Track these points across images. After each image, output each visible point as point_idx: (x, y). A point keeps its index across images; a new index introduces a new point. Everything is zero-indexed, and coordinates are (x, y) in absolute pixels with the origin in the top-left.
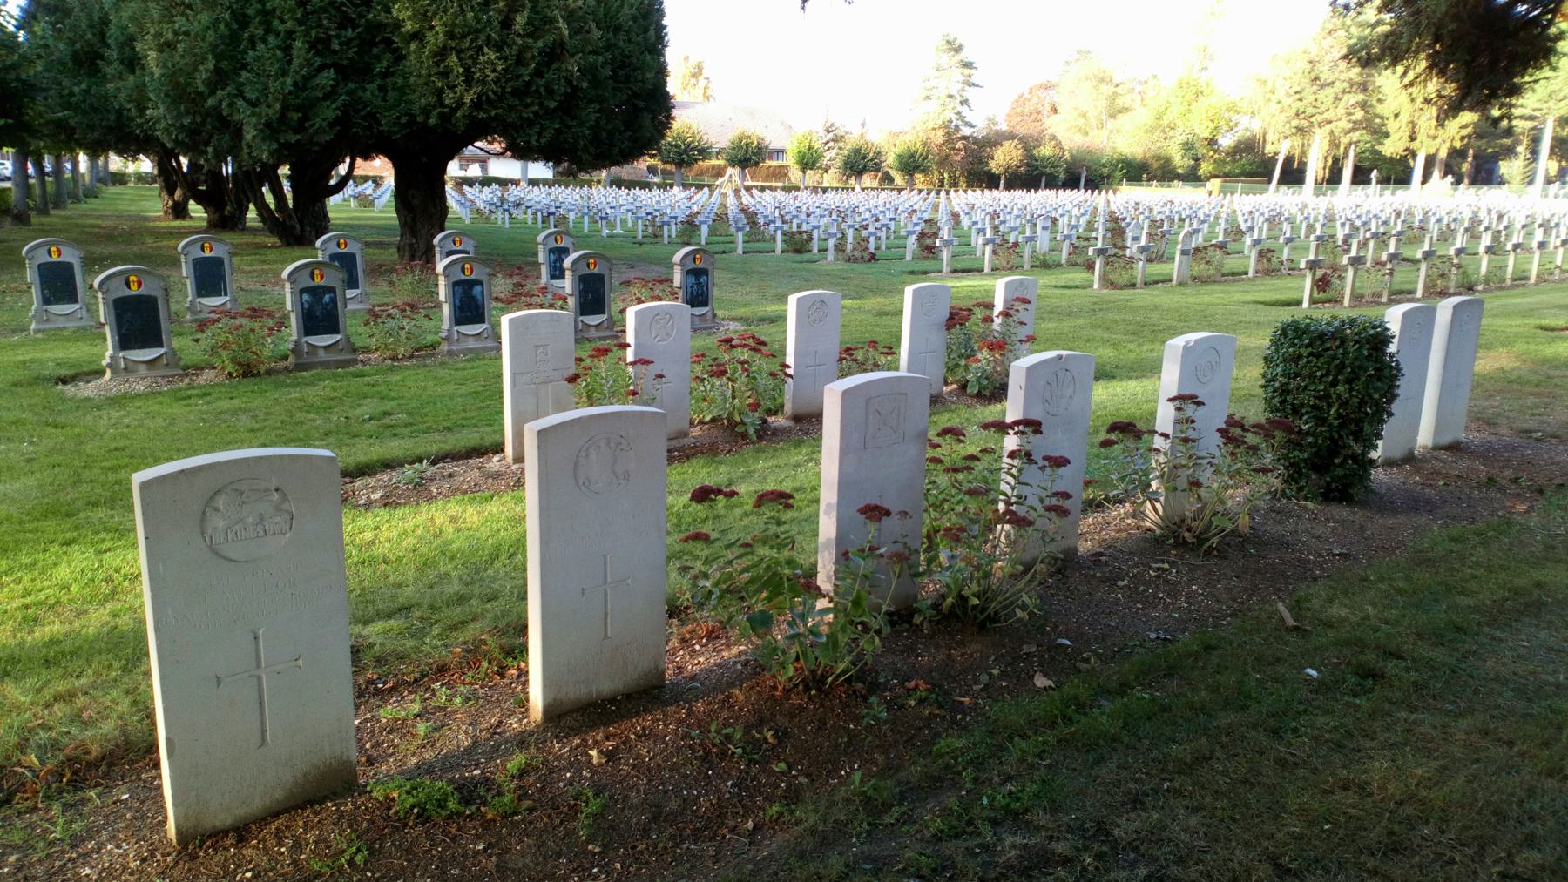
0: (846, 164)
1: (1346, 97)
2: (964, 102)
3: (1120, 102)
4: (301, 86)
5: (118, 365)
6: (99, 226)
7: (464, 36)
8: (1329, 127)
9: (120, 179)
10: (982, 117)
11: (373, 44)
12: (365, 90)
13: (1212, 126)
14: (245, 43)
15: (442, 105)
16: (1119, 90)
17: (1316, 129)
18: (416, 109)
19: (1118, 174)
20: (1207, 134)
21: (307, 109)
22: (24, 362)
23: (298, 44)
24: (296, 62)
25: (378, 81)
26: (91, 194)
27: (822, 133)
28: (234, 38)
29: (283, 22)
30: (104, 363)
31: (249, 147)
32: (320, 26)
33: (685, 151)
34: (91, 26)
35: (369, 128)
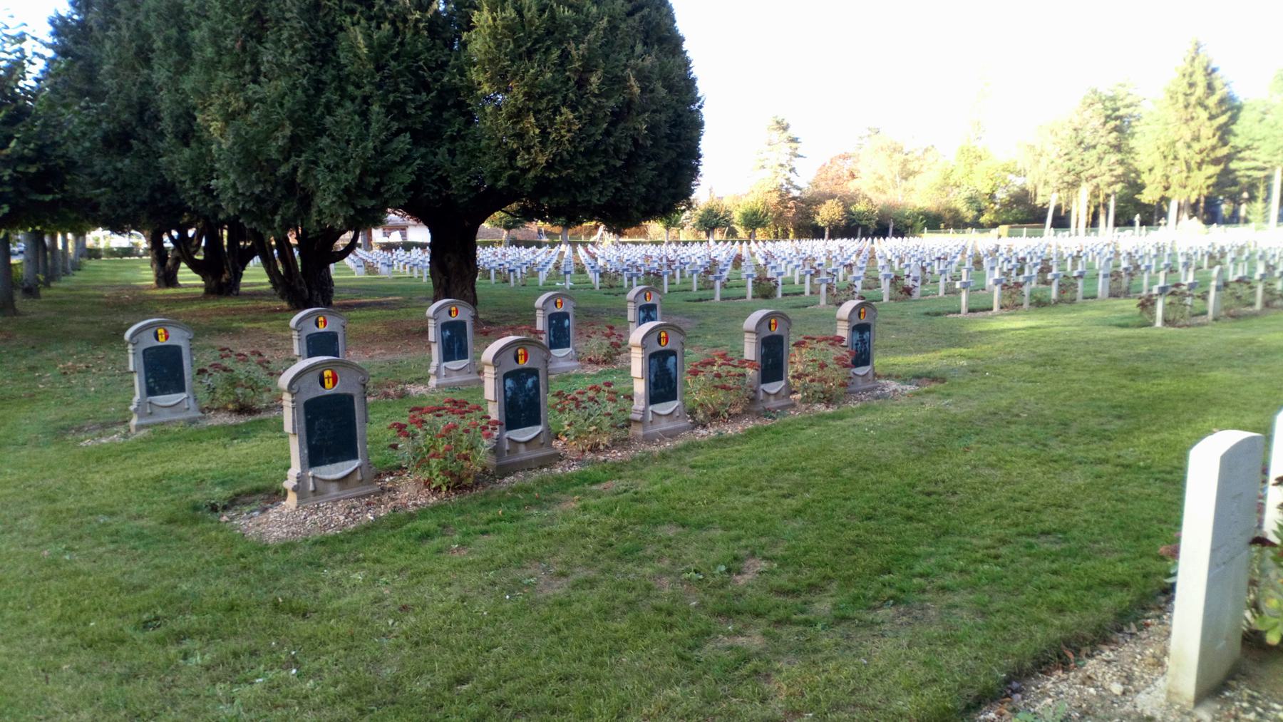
1: (1107, 157)
2: (792, 170)
3: (911, 167)
4: (379, 152)
5: (306, 486)
6: (102, 296)
7: (542, 96)
8: (1095, 181)
9: (94, 253)
10: (805, 180)
12: (435, 154)
13: (992, 183)
14: (321, 109)
15: (513, 167)
16: (909, 157)
17: (1084, 184)
18: (486, 172)
19: (919, 224)
20: (988, 190)
23: (375, 108)
24: (374, 127)
26: (77, 267)
28: (309, 105)
29: (358, 86)
31: (320, 212)
34: (129, 106)
35: (438, 192)
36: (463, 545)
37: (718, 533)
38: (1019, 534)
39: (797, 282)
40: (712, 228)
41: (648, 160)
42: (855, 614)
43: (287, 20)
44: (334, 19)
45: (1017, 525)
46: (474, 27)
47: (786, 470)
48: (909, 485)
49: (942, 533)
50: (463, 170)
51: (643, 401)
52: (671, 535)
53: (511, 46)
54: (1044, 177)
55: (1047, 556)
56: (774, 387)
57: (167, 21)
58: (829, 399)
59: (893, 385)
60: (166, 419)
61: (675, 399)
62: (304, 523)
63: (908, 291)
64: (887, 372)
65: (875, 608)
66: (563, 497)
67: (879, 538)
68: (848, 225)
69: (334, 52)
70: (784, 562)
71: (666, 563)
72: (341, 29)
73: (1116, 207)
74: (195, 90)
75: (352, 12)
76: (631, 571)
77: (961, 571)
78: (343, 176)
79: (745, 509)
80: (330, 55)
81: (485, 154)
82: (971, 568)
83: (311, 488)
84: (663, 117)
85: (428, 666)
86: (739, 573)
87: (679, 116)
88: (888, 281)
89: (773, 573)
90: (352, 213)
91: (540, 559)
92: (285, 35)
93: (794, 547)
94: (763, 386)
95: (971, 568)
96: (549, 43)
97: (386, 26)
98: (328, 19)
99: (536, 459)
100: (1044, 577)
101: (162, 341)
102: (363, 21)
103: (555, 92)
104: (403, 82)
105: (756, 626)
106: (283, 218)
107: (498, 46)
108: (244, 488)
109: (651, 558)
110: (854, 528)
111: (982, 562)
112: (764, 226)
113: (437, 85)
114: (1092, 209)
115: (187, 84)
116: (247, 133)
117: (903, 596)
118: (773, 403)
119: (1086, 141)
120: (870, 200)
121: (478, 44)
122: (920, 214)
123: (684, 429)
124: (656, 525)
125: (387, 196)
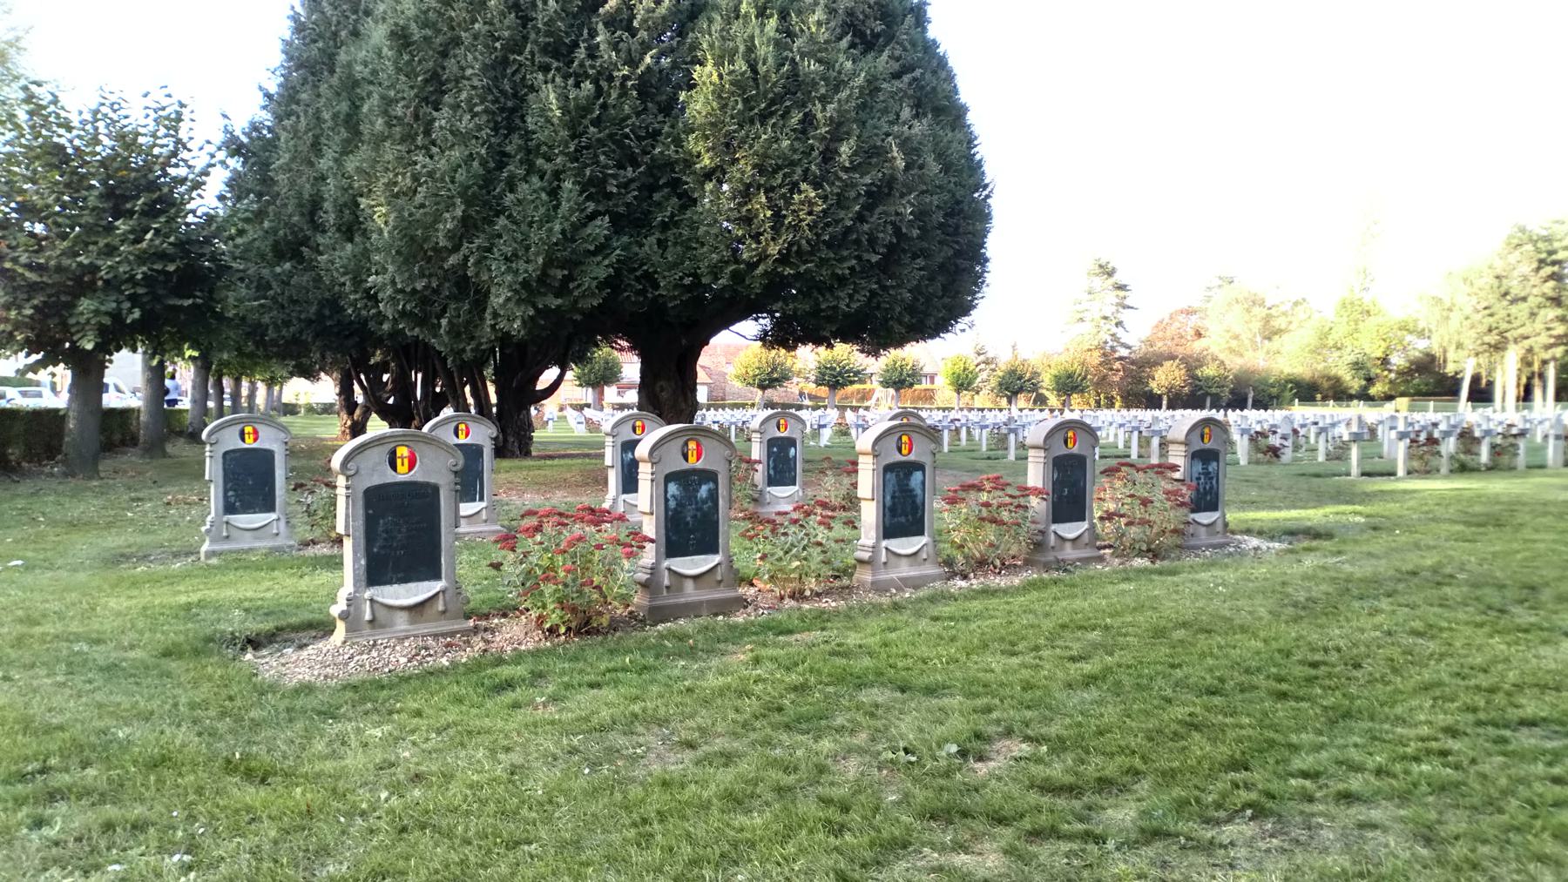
0: (1000, 384)
1: (1542, 312)
3: (1279, 323)
4: (568, 237)
5: (360, 612)
7: (775, 172)
8: (1526, 343)
9: (291, 409)
10: (1136, 335)
11: (653, 188)
12: (641, 246)
13: (1384, 345)
15: (737, 261)
16: (1273, 312)
18: (703, 267)
19: (1288, 394)
20: (1379, 354)
21: (573, 265)
22: (188, 607)
23: (568, 185)
24: (565, 206)
25: (657, 235)
27: (973, 356)
28: (488, 182)
29: (549, 160)
30: (335, 611)
31: (495, 315)
32: (597, 163)
33: (840, 374)
34: (300, 205)
35: (643, 292)
36: (554, 699)
37: (956, 701)
38: (1479, 723)
39: (1121, 446)
40: (1015, 393)
41: (915, 257)
42: (1182, 826)
43: (469, 79)
44: (524, 78)
45: (1475, 710)
46: (695, 86)
47: (1080, 628)
48: (1280, 651)
49: (1341, 716)
50: (675, 266)
51: (873, 534)
52: (880, 700)
53: (740, 106)
54: (1456, 338)
55: (1536, 755)
56: (1071, 530)
57: (338, 94)
58: (1154, 554)
59: (1254, 542)
60: (246, 546)
61: (921, 533)
62: (347, 664)
63: (1275, 452)
64: (1243, 527)
65: (1217, 823)
66: (731, 647)
67: (1229, 720)
68: (1192, 394)
69: (522, 118)
70: (1059, 746)
71: (862, 738)
72: (532, 89)
73: (1558, 379)
74: (359, 170)
75: (545, 69)
76: (801, 747)
77: (1379, 772)
78: (522, 265)
79: (1005, 672)
80: (518, 121)
81: (703, 244)
82: (1398, 767)
83: (368, 616)
84: (935, 200)
85: (401, 864)
86: (981, 758)
87: (958, 203)
88: (1246, 437)
89: (1039, 760)
90: (531, 312)
91: (663, 722)
92: (464, 95)
93: (1080, 725)
94: (1054, 527)
95: (1398, 767)
96: (788, 103)
97: (588, 86)
98: (518, 78)
99: (709, 602)
100: (1538, 787)
101: (249, 443)
102: (558, 80)
103: (792, 164)
104: (604, 153)
105: (993, 838)
106: (450, 322)
107: (723, 107)
108: (293, 620)
109: (840, 730)
110: (1184, 704)
111: (1417, 759)
112: (1082, 391)
113: (647, 159)
114: (1524, 380)
115: (351, 164)
116: (411, 215)
117: (1270, 804)
118: (1069, 553)
119: (1514, 292)
120: (1222, 362)
121: (698, 105)
122: (1287, 381)
123: (933, 579)
124: (859, 687)
125: (576, 293)
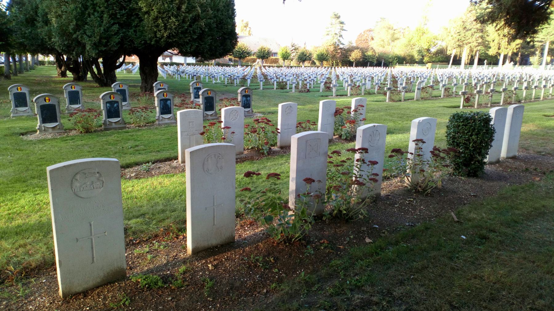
0: (299, 58)
1: (476, 34)
2: (341, 36)
3: (396, 36)
4: (106, 30)
5: (42, 129)
6: (35, 80)
7: (164, 13)
8: (469, 45)
9: (42, 63)
10: (347, 41)
11: (132, 15)
12: (129, 32)
13: (428, 44)
14: (86, 15)
15: (156, 37)
16: (395, 32)
17: (465, 46)
18: (147, 38)
19: (395, 61)
20: (426, 47)
21: (108, 38)
22: (9, 128)
23: (105, 15)
24: (105, 22)
25: (134, 29)
26: (32, 68)
27: (291, 47)
28: (83, 14)
29: (100, 8)
30: (37, 128)
31: (88, 52)
32: (113, 9)
33: (242, 53)
34: (32, 9)
35: (131, 45)
